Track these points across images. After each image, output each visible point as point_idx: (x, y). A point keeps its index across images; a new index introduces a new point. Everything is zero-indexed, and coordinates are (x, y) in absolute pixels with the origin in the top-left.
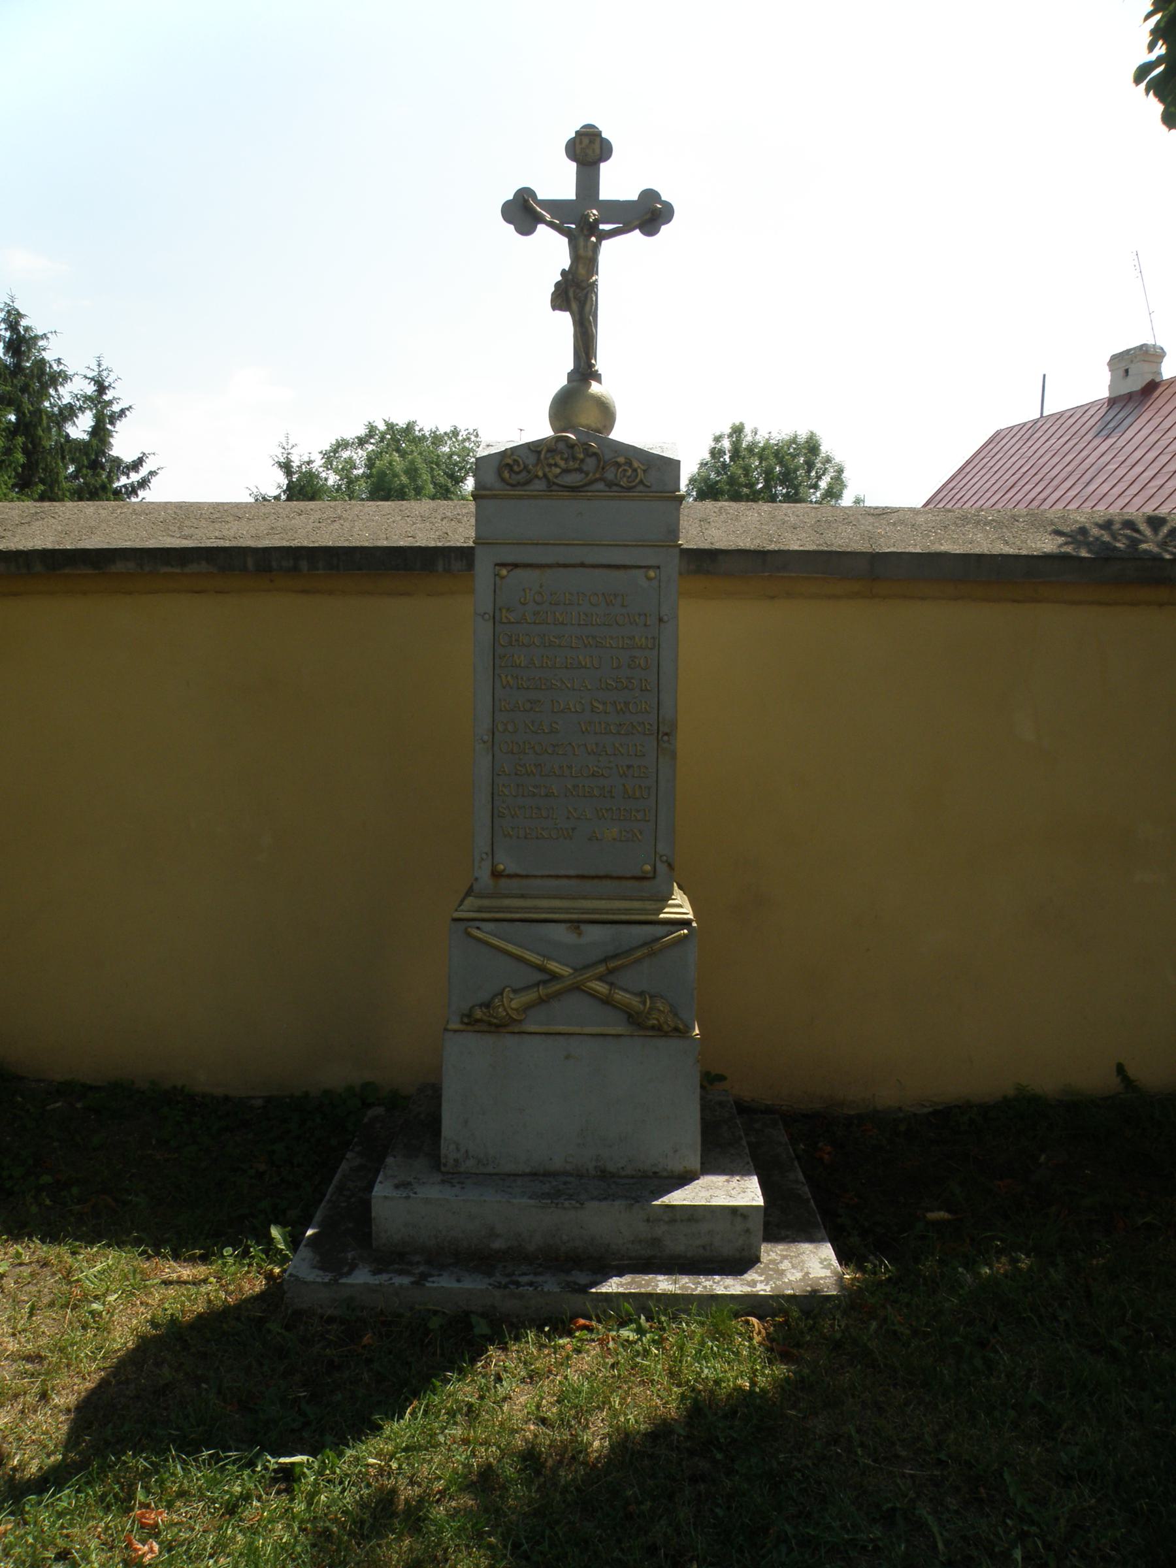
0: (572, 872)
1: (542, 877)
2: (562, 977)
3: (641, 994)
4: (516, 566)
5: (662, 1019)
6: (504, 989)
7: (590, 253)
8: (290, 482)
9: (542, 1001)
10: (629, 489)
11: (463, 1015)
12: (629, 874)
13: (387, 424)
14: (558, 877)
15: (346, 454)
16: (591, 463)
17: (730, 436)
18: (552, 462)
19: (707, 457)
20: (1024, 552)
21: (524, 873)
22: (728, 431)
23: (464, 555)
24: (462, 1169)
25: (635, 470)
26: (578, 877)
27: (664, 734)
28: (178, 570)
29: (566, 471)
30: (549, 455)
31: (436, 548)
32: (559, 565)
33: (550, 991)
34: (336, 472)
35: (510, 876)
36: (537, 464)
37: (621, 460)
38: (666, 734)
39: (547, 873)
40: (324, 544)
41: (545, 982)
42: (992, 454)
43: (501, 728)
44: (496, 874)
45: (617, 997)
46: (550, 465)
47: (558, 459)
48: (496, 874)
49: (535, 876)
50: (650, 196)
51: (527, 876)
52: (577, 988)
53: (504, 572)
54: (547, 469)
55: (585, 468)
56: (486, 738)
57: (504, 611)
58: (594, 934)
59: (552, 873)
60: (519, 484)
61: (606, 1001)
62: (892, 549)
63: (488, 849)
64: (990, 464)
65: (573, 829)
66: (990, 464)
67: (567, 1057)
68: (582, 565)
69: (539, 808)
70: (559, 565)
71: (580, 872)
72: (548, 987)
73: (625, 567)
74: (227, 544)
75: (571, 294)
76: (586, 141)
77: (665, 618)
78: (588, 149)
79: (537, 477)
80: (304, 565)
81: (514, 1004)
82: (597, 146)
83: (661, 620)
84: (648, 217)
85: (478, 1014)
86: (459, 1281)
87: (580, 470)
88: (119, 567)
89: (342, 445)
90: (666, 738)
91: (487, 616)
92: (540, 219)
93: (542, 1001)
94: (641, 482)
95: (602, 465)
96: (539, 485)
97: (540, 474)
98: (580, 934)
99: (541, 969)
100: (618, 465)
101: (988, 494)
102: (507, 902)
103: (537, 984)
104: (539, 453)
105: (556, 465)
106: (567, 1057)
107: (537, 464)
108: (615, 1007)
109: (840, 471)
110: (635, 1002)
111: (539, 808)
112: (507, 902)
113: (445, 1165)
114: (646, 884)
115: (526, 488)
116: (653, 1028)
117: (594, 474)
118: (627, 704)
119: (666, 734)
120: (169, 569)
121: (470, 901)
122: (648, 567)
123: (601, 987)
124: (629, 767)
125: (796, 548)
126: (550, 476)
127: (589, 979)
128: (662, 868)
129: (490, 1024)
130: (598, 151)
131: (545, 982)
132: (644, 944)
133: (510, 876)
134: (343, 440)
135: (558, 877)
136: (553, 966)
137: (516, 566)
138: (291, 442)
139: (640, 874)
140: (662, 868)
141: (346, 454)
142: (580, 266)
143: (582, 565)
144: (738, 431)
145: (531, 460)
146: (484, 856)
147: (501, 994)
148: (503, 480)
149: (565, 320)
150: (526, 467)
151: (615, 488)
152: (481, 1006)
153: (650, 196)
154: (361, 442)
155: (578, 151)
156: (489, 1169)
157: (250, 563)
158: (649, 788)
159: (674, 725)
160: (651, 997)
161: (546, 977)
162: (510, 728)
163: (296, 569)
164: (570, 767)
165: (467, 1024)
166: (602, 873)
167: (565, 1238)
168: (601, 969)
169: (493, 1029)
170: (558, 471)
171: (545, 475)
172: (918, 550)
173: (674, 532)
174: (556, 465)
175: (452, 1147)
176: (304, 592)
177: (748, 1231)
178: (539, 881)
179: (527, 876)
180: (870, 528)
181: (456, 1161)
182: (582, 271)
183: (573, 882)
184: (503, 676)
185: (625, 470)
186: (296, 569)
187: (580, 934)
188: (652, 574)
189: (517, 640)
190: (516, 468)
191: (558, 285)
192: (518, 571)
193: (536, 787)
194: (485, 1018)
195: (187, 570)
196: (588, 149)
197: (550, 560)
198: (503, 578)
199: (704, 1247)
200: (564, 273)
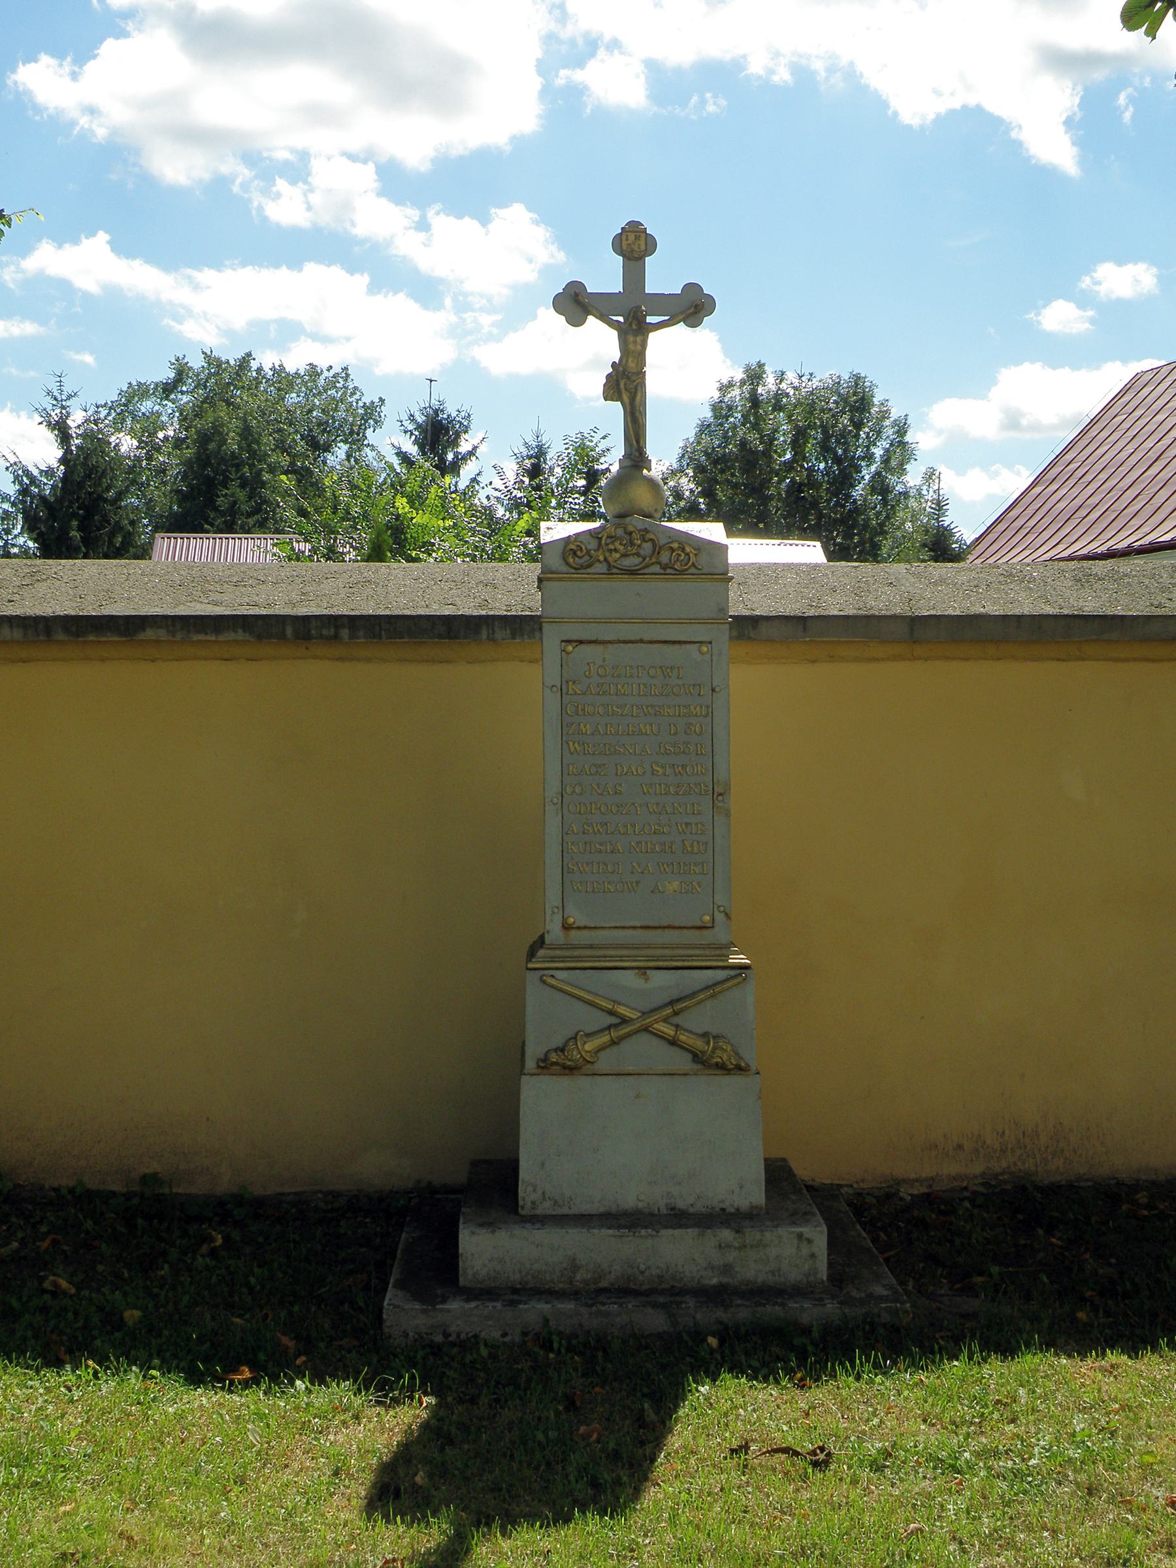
1: (610, 928)
2: (632, 1020)
3: (705, 1035)
4: (581, 642)
5: (725, 1057)
6: (577, 1034)
7: (639, 347)
8: (68, 451)
9: (613, 1043)
10: (682, 572)
11: (539, 1060)
12: (690, 924)
13: (208, 357)
14: (624, 928)
15: (147, 406)
16: (648, 547)
17: (743, 382)
18: (611, 547)
19: (708, 414)
20: (1066, 612)
22: (739, 375)
23: (521, 627)
24: (539, 1212)
25: (688, 554)
26: (641, 927)
27: (719, 794)
28: (213, 638)
29: (624, 555)
30: (609, 541)
32: (619, 642)
33: (621, 1033)
34: (132, 432)
35: (579, 928)
36: (597, 550)
37: (675, 545)
38: (721, 794)
39: (613, 925)
40: (365, 613)
41: (616, 1026)
42: (1129, 408)
43: (569, 790)
44: (566, 927)
45: (682, 1038)
46: (610, 551)
47: (617, 544)
48: (566, 927)
49: (634, 928)
50: (692, 288)
52: (646, 1029)
53: (570, 648)
54: (607, 554)
55: (642, 552)
56: (555, 800)
58: (659, 978)
60: (582, 567)
61: (673, 1043)
62: (932, 612)
63: (558, 903)
64: (1126, 425)
65: (637, 883)
66: (1126, 425)
67: (638, 1096)
68: (641, 641)
70: (619, 642)
72: (619, 1026)
74: (264, 612)
75: (622, 386)
76: (632, 237)
77: (717, 689)
78: (634, 245)
79: (598, 560)
80: (345, 633)
81: (588, 1047)
82: (642, 242)
83: (713, 690)
84: (692, 310)
85: (554, 1057)
87: (638, 554)
88: (149, 634)
89: (138, 392)
90: (720, 798)
91: (555, 689)
92: (587, 312)
93: (613, 1043)
94: (693, 564)
95: (657, 549)
96: (601, 568)
97: (601, 558)
98: (647, 980)
99: (611, 1013)
100: (673, 550)
101: (1124, 469)
102: (577, 953)
103: (609, 1027)
104: (600, 539)
105: (616, 550)
106: (638, 1096)
107: (597, 550)
108: (682, 1047)
109: (902, 429)
110: (699, 1044)
113: (523, 1207)
114: (705, 932)
115: (589, 570)
116: (717, 1064)
117: (651, 558)
118: (684, 767)
119: (721, 794)
120: (201, 637)
122: (701, 642)
123: (669, 1031)
124: (687, 824)
125: (836, 613)
126: (610, 559)
127: (656, 1021)
128: (720, 917)
129: (565, 1067)
130: (643, 247)
131: (616, 1026)
132: (708, 988)
133: (579, 928)
134: (139, 384)
135: (624, 928)
136: (621, 1010)
137: (581, 642)
138: (68, 389)
139: (699, 924)
140: (720, 917)
141: (147, 406)
142: (630, 360)
143: (641, 641)
144: (755, 375)
145: (593, 544)
147: (575, 1038)
148: (568, 564)
149: (617, 408)
150: (588, 552)
151: (669, 571)
152: (556, 1050)
153: (692, 288)
154: (168, 389)
155: (624, 247)
156: (565, 1211)
157: (289, 631)
158: (706, 843)
159: (727, 785)
160: (715, 1037)
161: (617, 1021)
162: (578, 790)
163: (336, 637)
165: (542, 1068)
167: (642, 1267)
168: (669, 1011)
169: (567, 1071)
170: (618, 555)
171: (605, 559)
172: (958, 613)
173: (723, 609)
174: (616, 550)
175: (530, 1189)
176: (341, 659)
177: (813, 1256)
178: (606, 933)
180: (910, 589)
181: (533, 1203)
182: (632, 364)
183: (638, 932)
185: (679, 555)
186: (336, 637)
187: (647, 980)
189: (583, 710)
190: (579, 553)
191: (609, 376)
192: (583, 647)
194: (560, 1061)
195: (221, 638)
196: (634, 245)
199: (773, 1273)
200: (614, 365)
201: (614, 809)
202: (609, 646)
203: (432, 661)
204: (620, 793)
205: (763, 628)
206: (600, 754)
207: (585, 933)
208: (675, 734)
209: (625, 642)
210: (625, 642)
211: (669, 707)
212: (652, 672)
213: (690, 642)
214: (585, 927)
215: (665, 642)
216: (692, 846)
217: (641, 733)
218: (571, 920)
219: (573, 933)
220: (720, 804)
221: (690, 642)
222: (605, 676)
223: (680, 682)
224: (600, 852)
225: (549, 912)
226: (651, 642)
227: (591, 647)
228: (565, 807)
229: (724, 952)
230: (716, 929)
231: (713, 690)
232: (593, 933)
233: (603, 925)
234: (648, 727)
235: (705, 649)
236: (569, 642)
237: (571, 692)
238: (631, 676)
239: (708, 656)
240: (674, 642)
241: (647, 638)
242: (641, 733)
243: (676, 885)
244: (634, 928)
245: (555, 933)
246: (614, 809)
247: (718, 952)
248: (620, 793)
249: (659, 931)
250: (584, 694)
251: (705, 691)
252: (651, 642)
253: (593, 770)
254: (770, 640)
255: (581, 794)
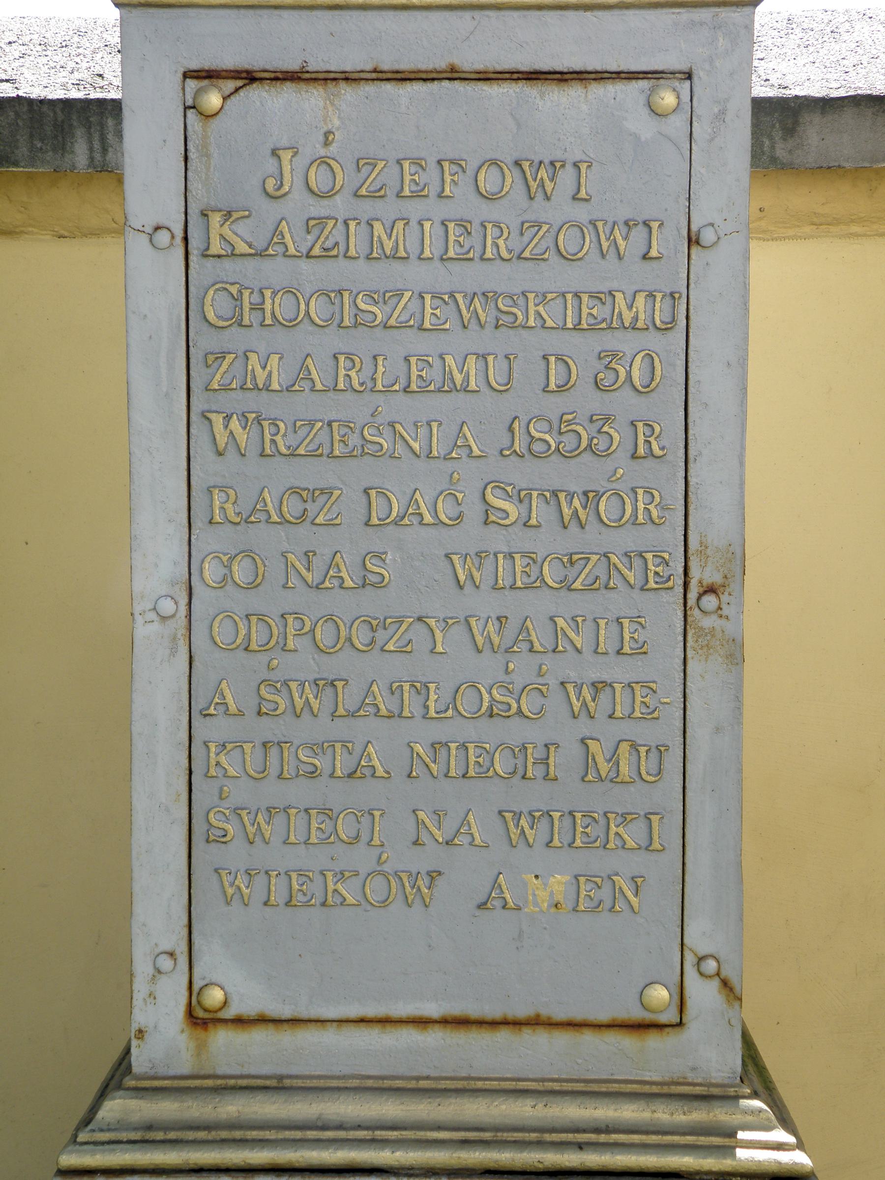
0: (432, 1010)
12: (603, 1017)
14: (385, 1021)
21: (287, 1012)
26: (446, 1022)
27: (703, 589)
31: (67, 103)
32: (380, 76)
35: (240, 1021)
38: (711, 590)
39: (354, 1011)
43: (211, 571)
44: (200, 1019)
49: (421, 1022)
51: (295, 1021)
53: (213, 100)
56: (167, 607)
57: (216, 219)
59: (371, 1011)
63: (176, 940)
65: (433, 875)
68: (453, 74)
69: (327, 812)
70: (380, 76)
71: (456, 1009)
73: (580, 76)
77: (708, 236)
83: (693, 241)
86: (684, 1114)
90: (710, 602)
91: (163, 237)
102: (231, 1108)
111: (327, 812)
112: (231, 1108)
114: (653, 1041)
118: (590, 497)
119: (711, 590)
121: (114, 1108)
124: (597, 687)
128: (703, 994)
133: (240, 1021)
135: (385, 1021)
139: (637, 1014)
140: (703, 994)
143: (453, 74)
146: (166, 963)
158: (661, 750)
159: (736, 559)
164: (422, 689)
166: (522, 1011)
178: (329, 1037)
179: (295, 1021)
183: (435, 1037)
184: (218, 420)
188: (668, 99)
189: (258, 307)
192: (256, 94)
193: (317, 748)
197: (353, 59)
198: (208, 117)
201: (361, 637)
202: (347, 92)
203: (740, 364)
204: (380, 585)
205: (814, 133)
206: (313, 455)
207: (259, 1035)
208: (562, 388)
209: (401, 77)
210: (401, 77)
211: (543, 299)
212: (488, 180)
213: (618, 75)
214: (263, 1020)
215: (533, 76)
216: (613, 758)
217: (448, 387)
218: (215, 996)
219: (222, 1039)
220: (707, 622)
221: (618, 75)
222: (328, 195)
223: (581, 213)
224: (313, 774)
225: (142, 968)
226: (485, 77)
227: (288, 92)
228: (199, 629)
229: (720, 1114)
230: (694, 1029)
231: (693, 241)
232: (288, 1038)
233: (314, 1013)
234: (472, 362)
235: (668, 99)
236: (210, 75)
237: (216, 247)
238: (417, 195)
239: (678, 123)
240: (561, 77)
241: (470, 61)
242: (448, 387)
243: (559, 883)
244: (421, 1022)
245: (162, 1036)
246: (361, 637)
247: (698, 1115)
248: (380, 585)
249: (503, 1035)
250: (260, 254)
251: (668, 242)
252: (485, 77)
253: (293, 506)
254: (828, 170)
255: (253, 586)
